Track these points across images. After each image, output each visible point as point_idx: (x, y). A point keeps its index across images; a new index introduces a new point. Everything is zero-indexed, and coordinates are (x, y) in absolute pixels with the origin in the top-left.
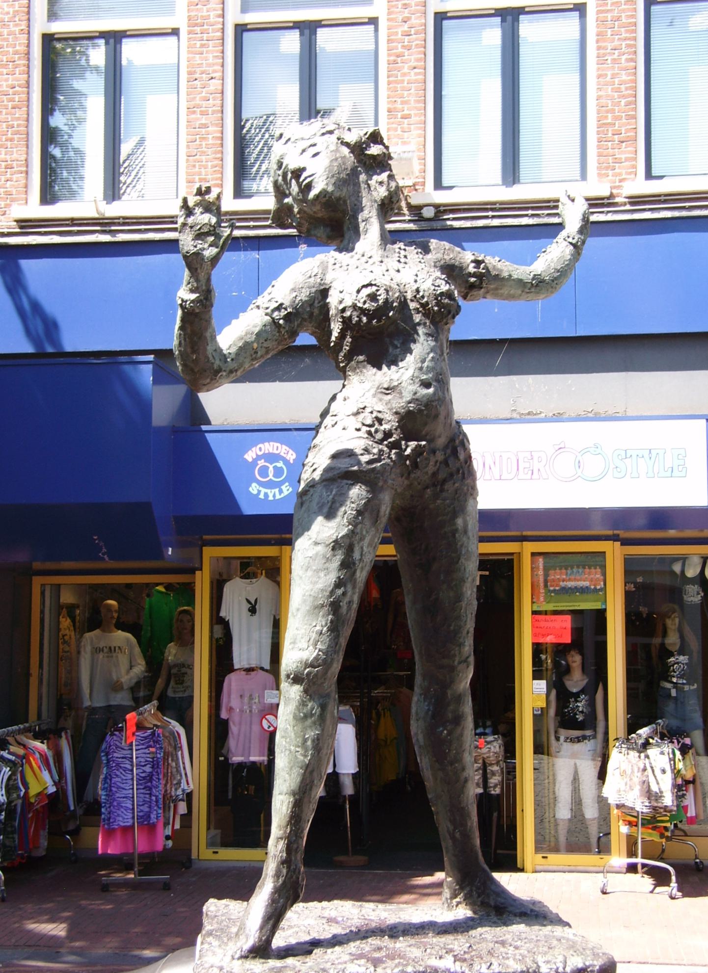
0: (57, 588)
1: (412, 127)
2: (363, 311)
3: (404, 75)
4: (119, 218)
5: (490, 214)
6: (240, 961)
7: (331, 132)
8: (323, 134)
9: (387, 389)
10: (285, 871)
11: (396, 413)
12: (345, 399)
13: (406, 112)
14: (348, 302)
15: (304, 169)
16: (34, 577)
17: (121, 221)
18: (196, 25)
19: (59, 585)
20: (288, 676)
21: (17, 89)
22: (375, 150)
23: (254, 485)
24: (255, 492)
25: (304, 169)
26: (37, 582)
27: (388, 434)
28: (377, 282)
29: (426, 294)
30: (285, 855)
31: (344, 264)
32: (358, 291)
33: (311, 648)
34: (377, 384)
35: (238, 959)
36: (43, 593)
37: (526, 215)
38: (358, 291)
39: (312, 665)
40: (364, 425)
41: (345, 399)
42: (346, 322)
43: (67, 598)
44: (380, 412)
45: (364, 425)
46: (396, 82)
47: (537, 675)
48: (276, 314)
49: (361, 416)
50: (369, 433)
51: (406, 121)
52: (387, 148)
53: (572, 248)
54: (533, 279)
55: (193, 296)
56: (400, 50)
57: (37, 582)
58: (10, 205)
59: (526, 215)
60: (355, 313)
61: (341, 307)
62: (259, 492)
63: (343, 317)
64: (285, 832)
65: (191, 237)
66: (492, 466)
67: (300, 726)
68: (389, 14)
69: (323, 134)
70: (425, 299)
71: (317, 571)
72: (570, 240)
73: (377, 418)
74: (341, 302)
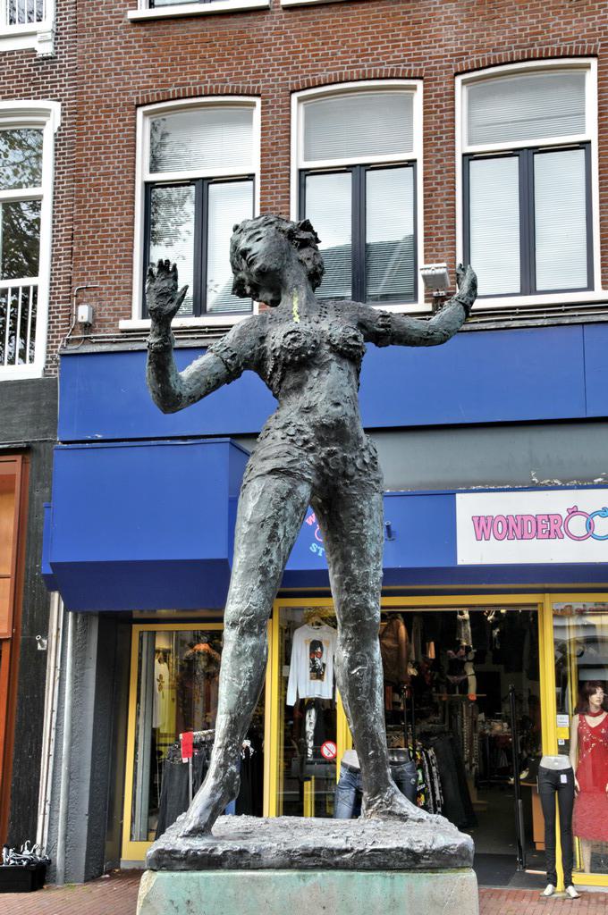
0: (153, 634)
1: (445, 247)
2: (288, 351)
3: (437, 206)
4: (204, 327)
5: (511, 317)
6: (182, 839)
7: (271, 223)
8: (266, 225)
9: (307, 408)
10: (222, 773)
11: (314, 426)
12: (276, 418)
13: (440, 236)
14: (278, 344)
15: (250, 250)
16: (134, 626)
17: (207, 330)
18: (268, 171)
19: (155, 632)
20: (228, 623)
21: (125, 226)
22: (304, 235)
23: (313, 545)
24: (315, 551)
25: (250, 250)
26: (137, 628)
27: (306, 442)
28: (300, 330)
29: (338, 338)
30: (222, 760)
31: (278, 318)
32: (285, 337)
33: (244, 602)
34: (299, 405)
35: (181, 837)
36: (141, 639)
37: (542, 318)
38: (285, 337)
39: (245, 614)
40: (288, 435)
41: (276, 418)
42: (276, 358)
43: (162, 644)
44: (301, 425)
45: (288, 435)
46: (431, 212)
47: (561, 708)
48: (225, 355)
49: (286, 431)
50: (292, 441)
51: (440, 243)
52: (315, 234)
53: (461, 306)
54: (429, 329)
55: (157, 340)
56: (434, 186)
57: (137, 628)
58: (118, 320)
59: (542, 318)
60: (283, 353)
61: (273, 348)
62: (318, 550)
63: (274, 356)
64: (223, 743)
65: (154, 296)
66: (515, 526)
67: (236, 660)
68: (425, 157)
69: (266, 225)
70: (337, 342)
71: (250, 544)
72: (460, 300)
73: (299, 430)
74: (273, 345)
